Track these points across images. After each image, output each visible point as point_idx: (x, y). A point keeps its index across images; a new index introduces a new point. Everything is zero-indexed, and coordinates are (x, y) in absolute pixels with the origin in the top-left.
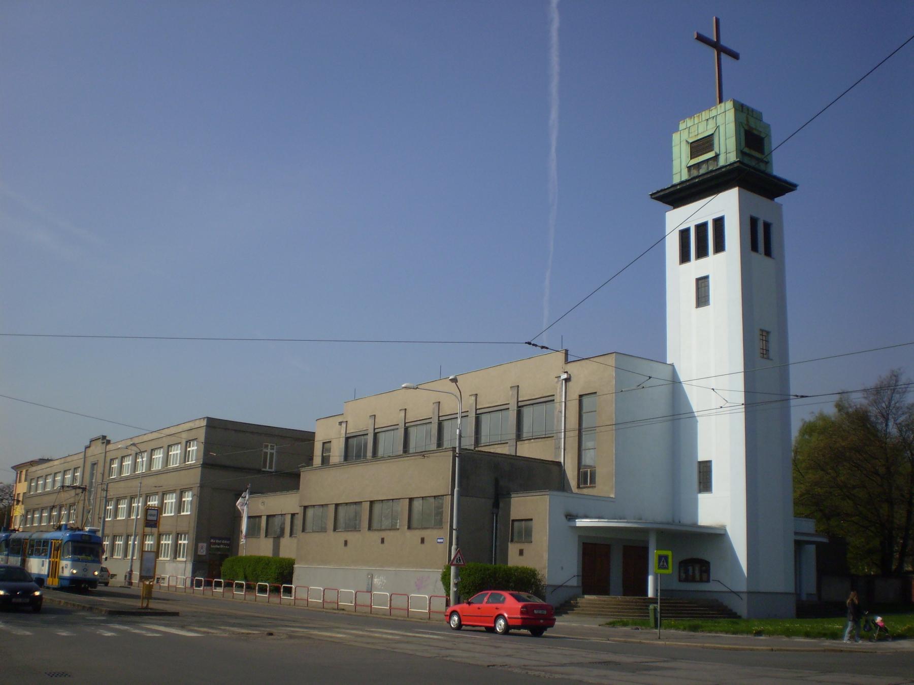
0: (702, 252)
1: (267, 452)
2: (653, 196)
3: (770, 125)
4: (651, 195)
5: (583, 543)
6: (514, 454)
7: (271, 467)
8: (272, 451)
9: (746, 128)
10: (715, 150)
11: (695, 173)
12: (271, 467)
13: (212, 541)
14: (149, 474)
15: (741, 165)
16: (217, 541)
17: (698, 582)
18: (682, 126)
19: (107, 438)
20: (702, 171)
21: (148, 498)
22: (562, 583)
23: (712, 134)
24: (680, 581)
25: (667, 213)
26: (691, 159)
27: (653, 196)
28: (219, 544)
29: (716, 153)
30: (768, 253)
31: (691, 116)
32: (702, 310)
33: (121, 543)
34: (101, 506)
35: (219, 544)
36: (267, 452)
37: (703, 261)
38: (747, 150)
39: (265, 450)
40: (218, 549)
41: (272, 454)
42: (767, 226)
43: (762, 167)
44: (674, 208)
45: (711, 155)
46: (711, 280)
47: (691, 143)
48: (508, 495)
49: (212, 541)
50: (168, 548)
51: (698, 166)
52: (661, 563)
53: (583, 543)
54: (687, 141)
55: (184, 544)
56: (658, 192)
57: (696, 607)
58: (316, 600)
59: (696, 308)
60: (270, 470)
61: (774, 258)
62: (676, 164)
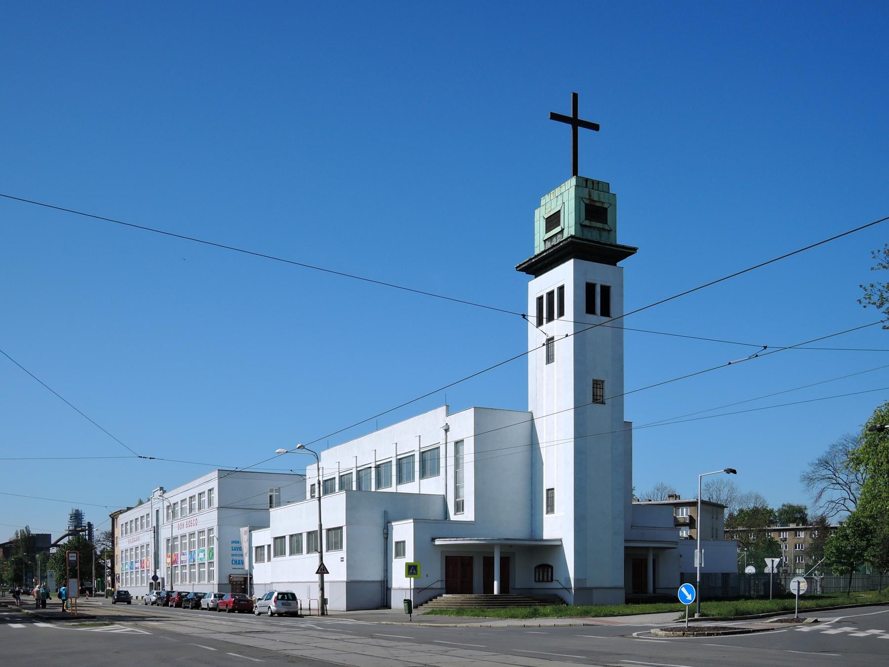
2: (518, 269)
4: (517, 268)
5: (446, 557)
6: (418, 493)
9: (587, 202)
11: (549, 245)
15: (573, 240)
18: (543, 202)
23: (560, 210)
25: (529, 283)
26: (546, 233)
27: (518, 269)
29: (562, 228)
31: (548, 192)
34: (293, 547)
38: (587, 223)
42: (606, 290)
44: (536, 277)
45: (558, 229)
47: (546, 219)
48: (390, 522)
51: (550, 238)
52: (411, 571)
53: (446, 557)
54: (543, 217)
56: (520, 265)
57: (521, 598)
58: (749, 601)
59: (546, 364)
62: (537, 237)
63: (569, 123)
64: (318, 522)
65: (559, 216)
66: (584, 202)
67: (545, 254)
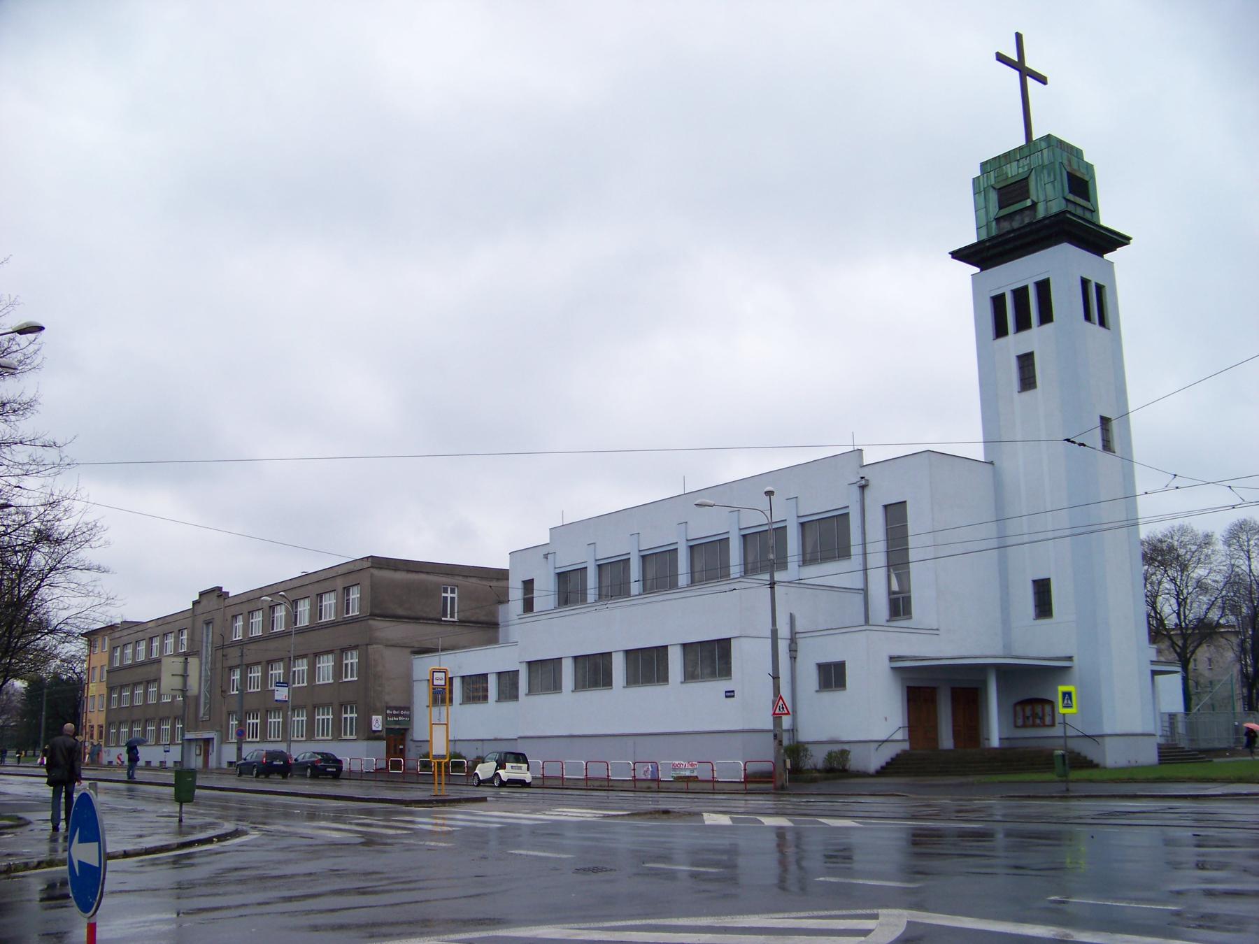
0: (1023, 323)
1: (447, 597)
3: (1093, 166)
7: (452, 616)
8: (453, 595)
10: (1031, 197)
11: (1006, 226)
12: (452, 616)
13: (388, 712)
14: (269, 637)
16: (395, 712)
17: (1048, 726)
19: (224, 590)
20: (1016, 225)
21: (344, 654)
22: (887, 737)
23: (1027, 178)
24: (1016, 726)
28: (397, 716)
29: (1033, 201)
30: (1102, 323)
32: (1028, 395)
33: (140, 729)
35: (397, 716)
36: (447, 597)
37: (1024, 334)
39: (444, 595)
40: (397, 722)
41: (452, 599)
42: (1100, 289)
43: (1088, 215)
45: (1028, 203)
46: (1051, 279)
47: (999, 189)
49: (388, 712)
50: (302, 726)
51: (1010, 216)
52: (1066, 702)
55: (351, 719)
60: (451, 619)
61: (1109, 329)
63: (1027, 68)
64: (770, 626)
65: (1027, 186)
66: (1066, 169)
67: (1012, 235)
